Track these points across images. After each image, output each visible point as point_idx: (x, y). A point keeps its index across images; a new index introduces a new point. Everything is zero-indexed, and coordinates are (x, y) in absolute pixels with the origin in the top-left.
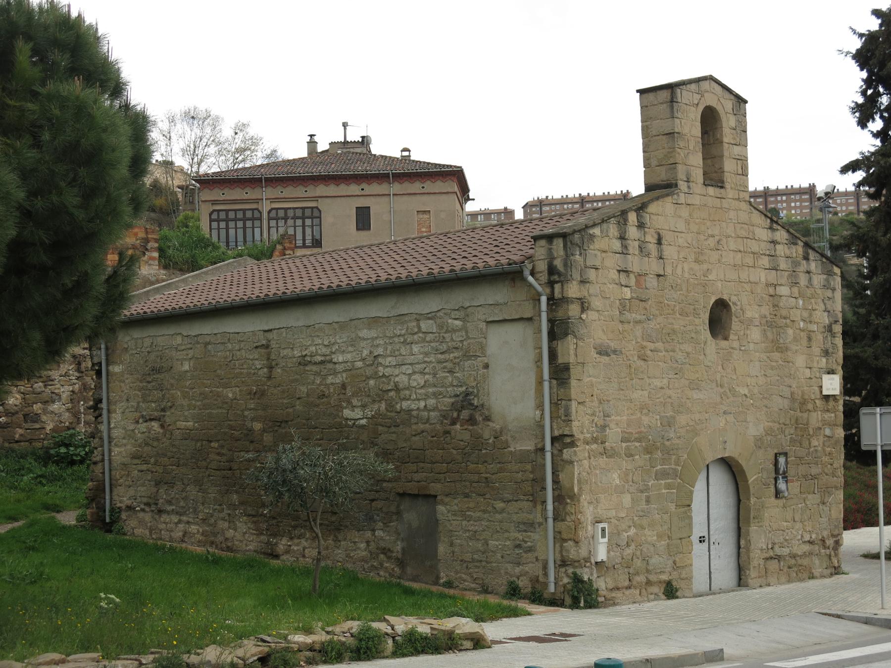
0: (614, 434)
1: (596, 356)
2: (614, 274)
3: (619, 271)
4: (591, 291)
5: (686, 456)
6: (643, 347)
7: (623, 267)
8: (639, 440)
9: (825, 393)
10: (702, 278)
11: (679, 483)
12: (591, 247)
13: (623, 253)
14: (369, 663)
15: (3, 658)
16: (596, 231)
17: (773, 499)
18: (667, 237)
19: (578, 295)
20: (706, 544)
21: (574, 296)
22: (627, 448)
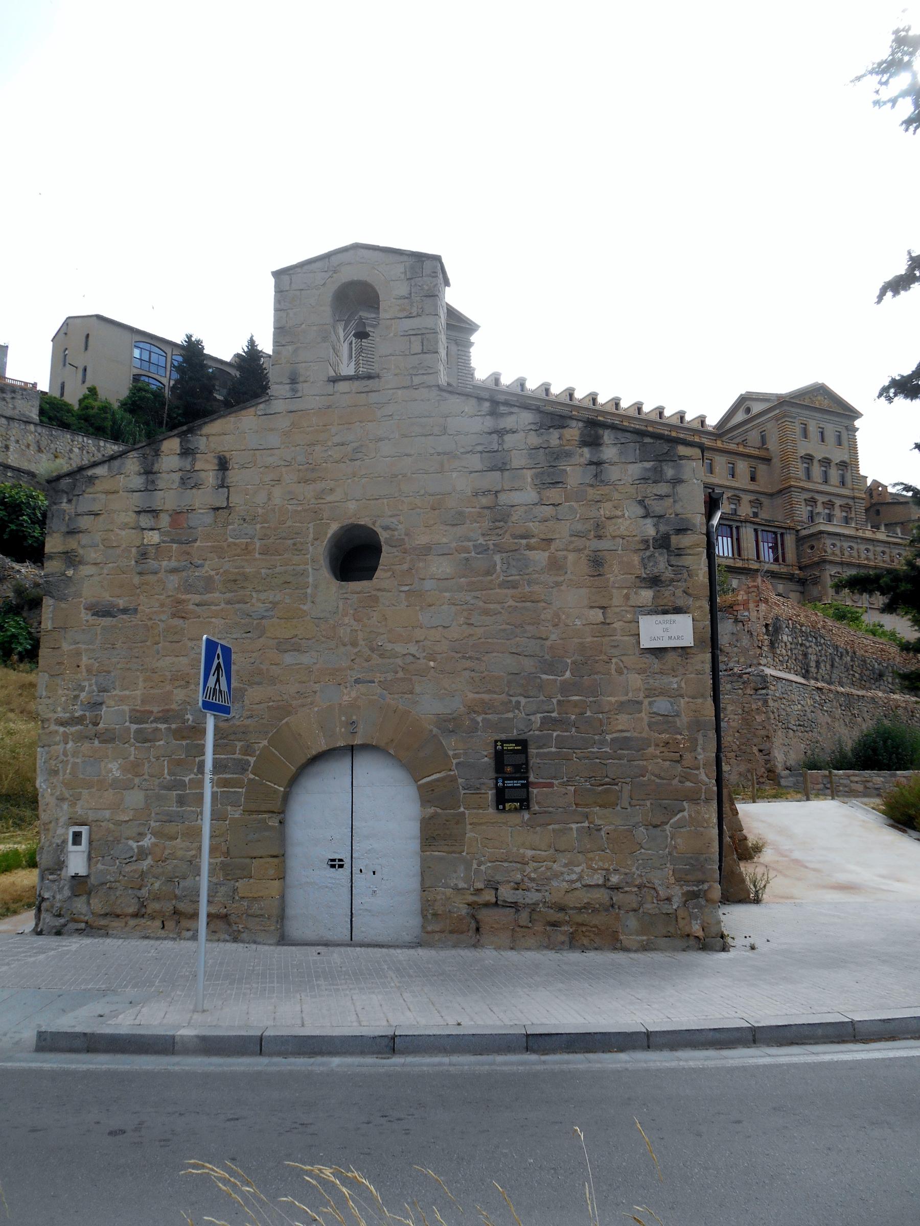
0: (112, 715)
1: (89, 617)
2: (130, 518)
3: (139, 513)
4: (83, 542)
5: (265, 742)
6: (179, 602)
7: (145, 506)
8: (165, 720)
9: (645, 643)
10: (313, 501)
11: (250, 780)
12: (88, 490)
13: (146, 490)
14: (361, 279)
15: (919, 498)
16: (100, 471)
17: (491, 810)
18: (236, 459)
19: (60, 549)
20: (343, 873)
21: (55, 550)
22: (138, 731)
